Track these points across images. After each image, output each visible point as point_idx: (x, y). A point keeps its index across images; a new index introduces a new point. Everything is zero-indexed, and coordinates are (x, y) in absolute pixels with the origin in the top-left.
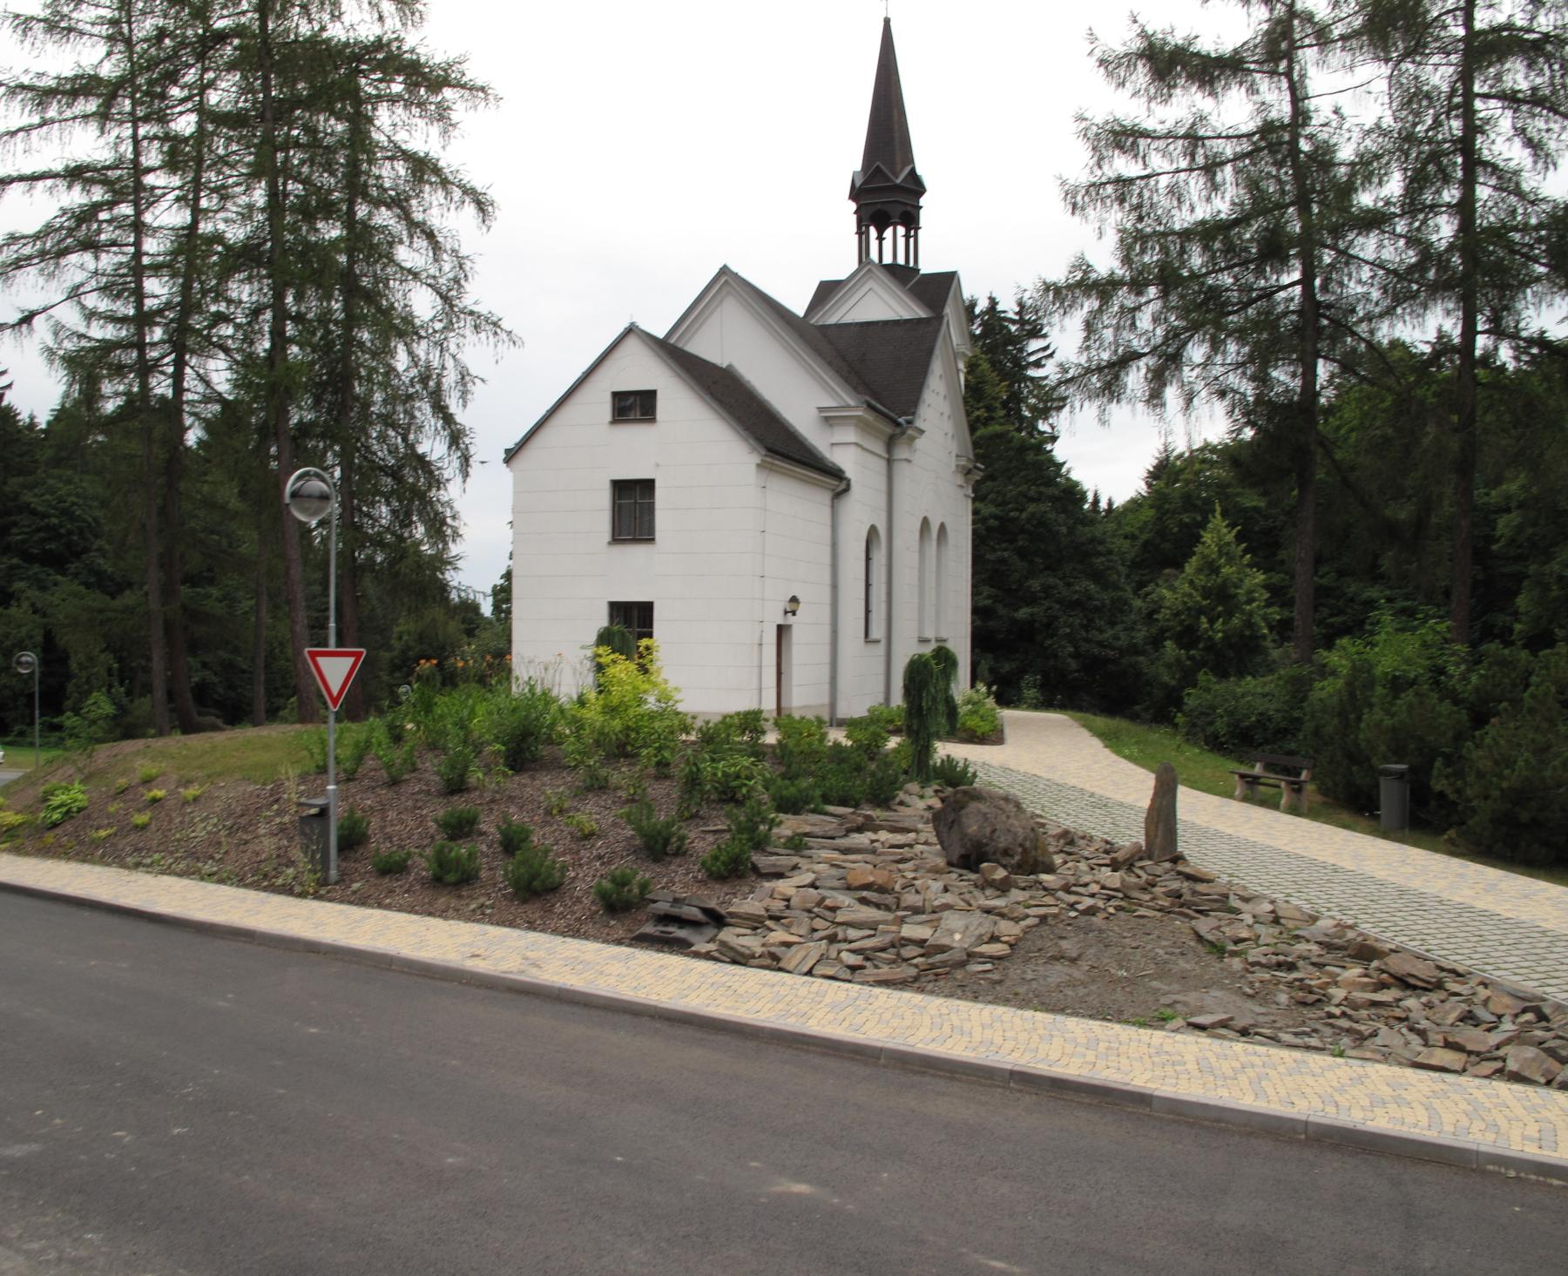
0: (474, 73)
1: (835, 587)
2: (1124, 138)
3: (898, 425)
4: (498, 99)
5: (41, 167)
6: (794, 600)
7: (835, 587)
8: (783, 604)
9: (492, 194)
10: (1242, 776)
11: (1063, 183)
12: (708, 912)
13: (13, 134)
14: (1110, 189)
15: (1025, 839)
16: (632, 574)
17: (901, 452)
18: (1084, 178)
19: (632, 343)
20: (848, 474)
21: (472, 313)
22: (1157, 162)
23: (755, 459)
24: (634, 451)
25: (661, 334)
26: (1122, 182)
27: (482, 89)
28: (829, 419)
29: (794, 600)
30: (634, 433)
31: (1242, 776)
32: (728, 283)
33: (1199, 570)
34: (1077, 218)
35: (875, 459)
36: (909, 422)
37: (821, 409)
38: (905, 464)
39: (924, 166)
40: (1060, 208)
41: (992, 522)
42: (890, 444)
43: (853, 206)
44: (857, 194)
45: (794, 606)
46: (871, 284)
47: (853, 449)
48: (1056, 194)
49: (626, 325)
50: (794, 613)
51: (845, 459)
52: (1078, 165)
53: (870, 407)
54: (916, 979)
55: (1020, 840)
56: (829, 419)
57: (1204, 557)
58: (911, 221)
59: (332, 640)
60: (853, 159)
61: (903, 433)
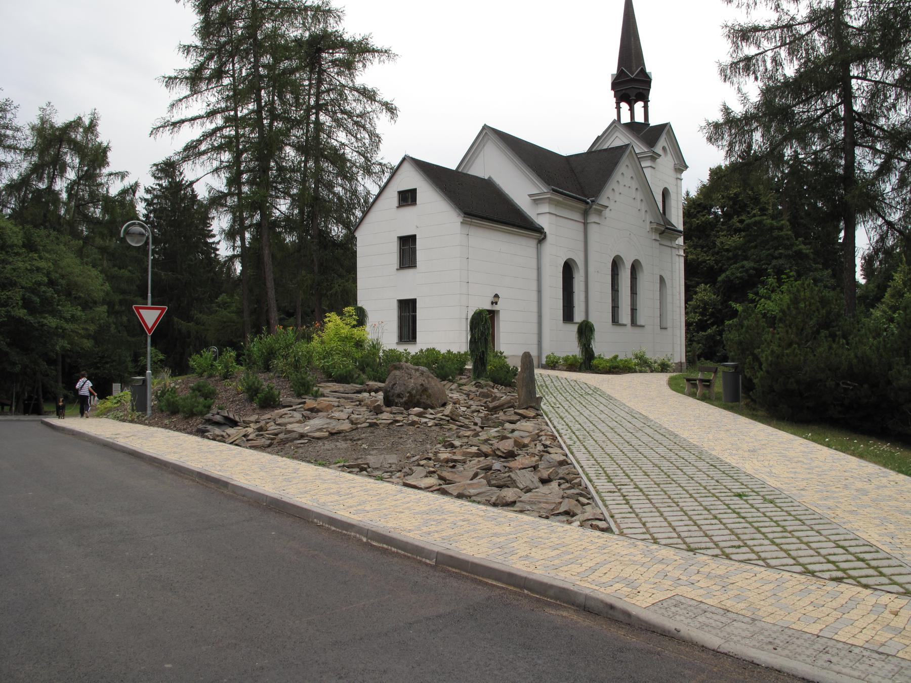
0: (376, 42)
1: (539, 291)
2: (744, 34)
3: (587, 203)
4: (395, 55)
5: (196, 114)
6: (496, 296)
7: (539, 291)
8: (490, 298)
9: (396, 104)
10: (688, 380)
11: (720, 65)
12: (227, 418)
13: (180, 100)
14: (741, 65)
15: (413, 389)
16: (408, 285)
17: (593, 218)
18: (727, 60)
19: (406, 165)
20: (546, 230)
21: (380, 164)
22: (765, 45)
23: (460, 219)
24: (408, 221)
25: (452, 164)
26: (748, 59)
27: (386, 51)
28: (536, 200)
29: (496, 296)
30: (408, 211)
31: (688, 380)
32: (489, 134)
33: (892, 296)
34: (728, 83)
35: (577, 223)
36: (593, 201)
37: (530, 196)
38: (594, 226)
39: (650, 67)
40: (718, 78)
41: (751, 271)
42: (585, 214)
43: (613, 92)
44: (615, 85)
45: (496, 300)
46: (617, 134)
47: (548, 215)
48: (716, 70)
49: (403, 156)
50: (496, 303)
51: (543, 221)
52: (724, 52)
53: (554, 190)
54: (269, 446)
55: (409, 390)
56: (536, 200)
57: (895, 288)
58: (643, 96)
59: (149, 301)
60: (612, 67)
61: (591, 207)
